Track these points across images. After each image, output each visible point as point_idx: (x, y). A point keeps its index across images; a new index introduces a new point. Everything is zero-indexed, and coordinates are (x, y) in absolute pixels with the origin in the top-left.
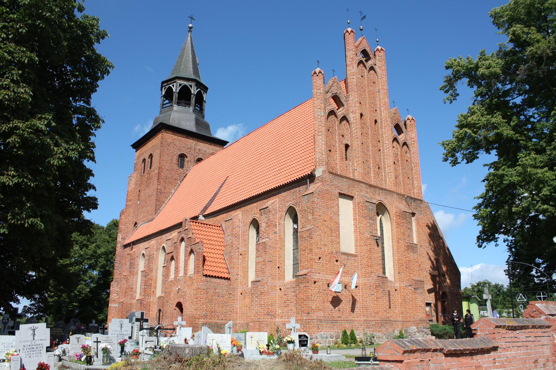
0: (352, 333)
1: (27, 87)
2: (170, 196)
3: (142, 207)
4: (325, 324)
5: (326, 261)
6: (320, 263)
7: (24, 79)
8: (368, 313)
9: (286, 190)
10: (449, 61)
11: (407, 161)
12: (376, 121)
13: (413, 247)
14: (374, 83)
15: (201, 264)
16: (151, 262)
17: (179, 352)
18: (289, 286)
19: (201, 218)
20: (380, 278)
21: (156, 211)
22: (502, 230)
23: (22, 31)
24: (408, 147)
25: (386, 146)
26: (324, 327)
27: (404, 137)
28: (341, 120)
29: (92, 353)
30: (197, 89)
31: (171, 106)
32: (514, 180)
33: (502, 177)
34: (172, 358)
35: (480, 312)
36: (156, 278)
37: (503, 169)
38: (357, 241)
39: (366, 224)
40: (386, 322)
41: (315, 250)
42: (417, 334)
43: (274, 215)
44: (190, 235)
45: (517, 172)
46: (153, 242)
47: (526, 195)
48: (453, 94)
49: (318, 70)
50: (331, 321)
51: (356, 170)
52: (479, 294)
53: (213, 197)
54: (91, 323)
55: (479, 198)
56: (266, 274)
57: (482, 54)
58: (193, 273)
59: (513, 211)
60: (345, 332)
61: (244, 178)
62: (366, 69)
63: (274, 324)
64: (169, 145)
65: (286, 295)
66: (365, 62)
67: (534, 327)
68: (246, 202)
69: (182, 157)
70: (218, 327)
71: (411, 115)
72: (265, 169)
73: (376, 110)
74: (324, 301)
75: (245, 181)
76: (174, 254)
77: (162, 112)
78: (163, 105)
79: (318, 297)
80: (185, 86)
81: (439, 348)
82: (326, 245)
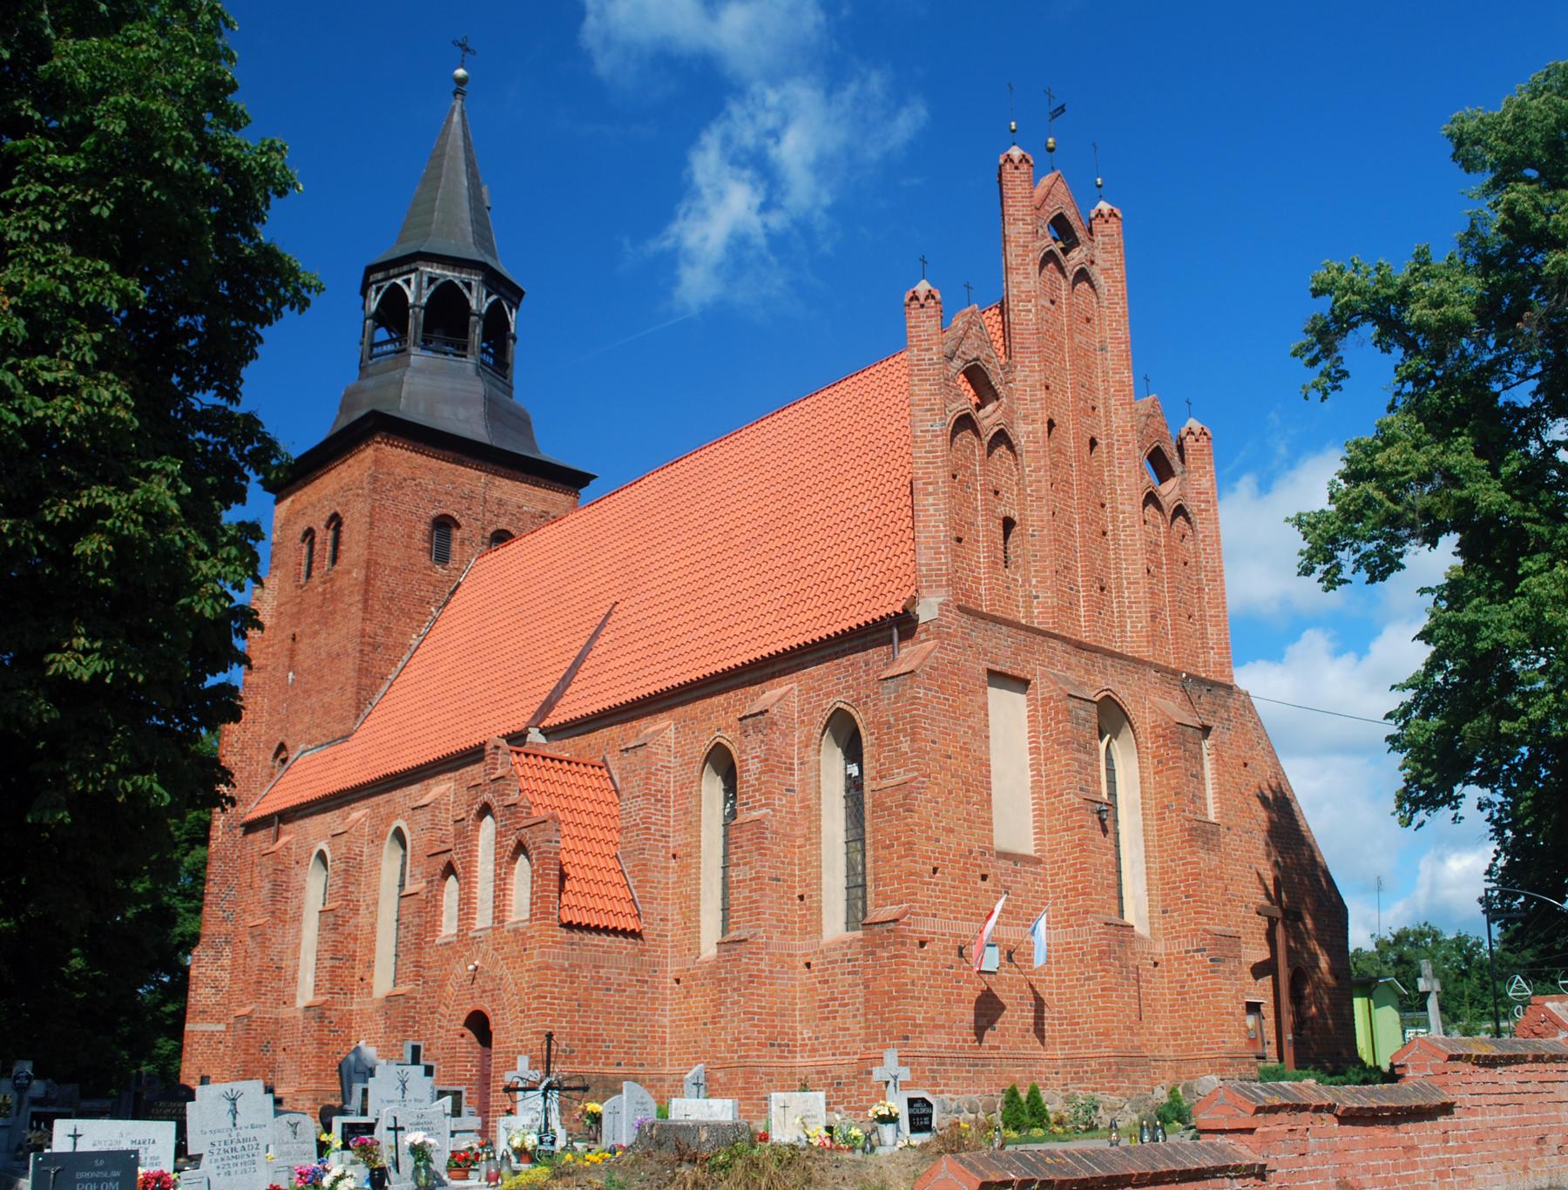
0: (1034, 1095)
1: (118, 383)
2: (405, 658)
3: (306, 691)
4: (953, 1071)
5: (953, 880)
6: (937, 885)
7: (107, 359)
8: (1077, 1036)
9: (824, 657)
10: (1322, 273)
11: (1185, 564)
12: (1093, 443)
13: (1206, 832)
14: (1088, 320)
15: (553, 887)
16: (352, 880)
18: (837, 955)
19: (535, 736)
20: (1112, 930)
21: (358, 708)
22: (1474, 773)
23: (99, 214)
24: (1188, 520)
25: (1124, 521)
26: (950, 1079)
27: (1177, 491)
31: (404, 350)
32: (1508, 640)
33: (1472, 629)
34: (668, 1154)
35: (1404, 1032)
36: (373, 932)
37: (1476, 607)
38: (1041, 816)
39: (1068, 765)
40: (1130, 1062)
41: (923, 847)
43: (785, 735)
44: (514, 797)
45: (1516, 616)
46: (358, 813)
47: (1541, 685)
48: (1333, 371)
50: (971, 1061)
51: (1037, 597)
52: (1400, 970)
53: (570, 669)
54: (513, 1067)
55: (1403, 687)
56: (765, 920)
57: (1422, 258)
58: (527, 916)
59: (1503, 730)
60: (1013, 1093)
62: (1065, 277)
63: (791, 1074)
64: (399, 487)
65: (826, 982)
66: (1060, 255)
67: (1538, 1059)
68: (691, 690)
69: (444, 525)
70: (605, 1087)
72: (746, 584)
73: (1094, 408)
74: (949, 1001)
75: (681, 620)
77: (370, 370)
78: (373, 345)
79: (931, 987)
80: (450, 284)
81: (1326, 1103)
82: (952, 831)
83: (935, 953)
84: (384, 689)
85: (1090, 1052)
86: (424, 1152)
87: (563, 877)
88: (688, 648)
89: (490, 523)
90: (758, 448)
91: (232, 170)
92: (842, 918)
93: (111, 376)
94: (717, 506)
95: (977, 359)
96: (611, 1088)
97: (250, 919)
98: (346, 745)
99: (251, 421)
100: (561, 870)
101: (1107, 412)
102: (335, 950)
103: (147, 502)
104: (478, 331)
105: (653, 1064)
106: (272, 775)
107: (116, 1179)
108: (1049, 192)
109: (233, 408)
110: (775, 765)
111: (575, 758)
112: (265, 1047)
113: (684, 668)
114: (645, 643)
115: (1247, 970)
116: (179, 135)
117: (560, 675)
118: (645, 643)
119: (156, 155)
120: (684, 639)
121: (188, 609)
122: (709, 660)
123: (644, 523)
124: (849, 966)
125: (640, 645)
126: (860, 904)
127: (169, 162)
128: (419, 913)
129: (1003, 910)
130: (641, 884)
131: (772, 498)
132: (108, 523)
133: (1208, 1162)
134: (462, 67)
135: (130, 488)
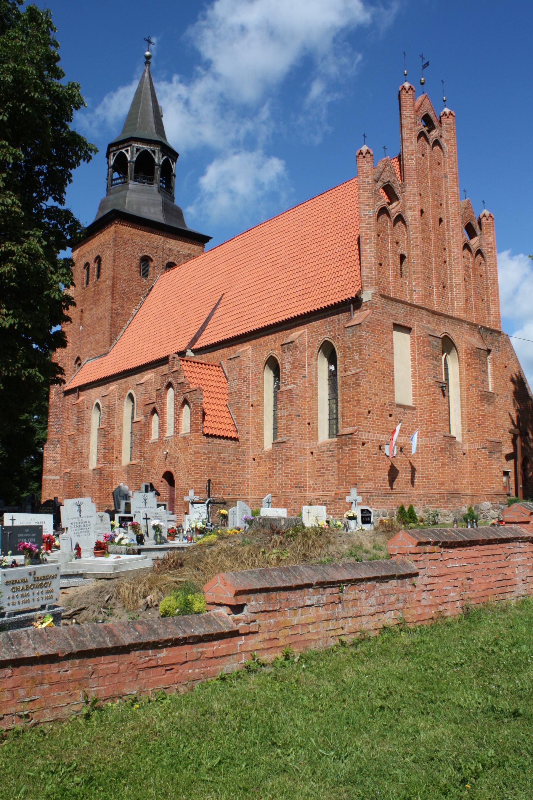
0: (411, 509)
2: (130, 319)
3: (88, 334)
12: (441, 220)
13: (488, 396)
14: (439, 164)
15: (200, 418)
17: (275, 524)
18: (325, 449)
19: (189, 353)
20: (446, 439)
24: (483, 256)
27: (478, 243)
28: (395, 220)
29: (143, 531)
30: (163, 157)
31: (126, 182)
34: (267, 530)
42: (492, 511)
46: (113, 387)
49: (364, 148)
51: (415, 291)
53: (204, 324)
54: (187, 495)
58: (189, 431)
60: (402, 508)
61: (251, 298)
62: (429, 143)
64: (126, 243)
65: (320, 460)
69: (145, 260)
71: (488, 210)
72: (283, 285)
73: (441, 205)
74: (374, 469)
75: (253, 301)
76: (157, 405)
77: (112, 191)
80: (146, 151)
82: (377, 395)
83: (369, 448)
84: (121, 333)
85: (436, 491)
86: (159, 529)
87: (204, 414)
88: (257, 314)
89: (166, 259)
90: (287, 224)
91: (56, 97)
92: (327, 432)
93: (11, 193)
94: (269, 250)
95: (389, 182)
96: (234, 503)
97: (68, 432)
98: (106, 358)
99: (68, 214)
100: (203, 411)
101: (447, 206)
102: (105, 445)
103: (30, 249)
104: (159, 173)
105: (243, 495)
106: (74, 371)
107: (34, 537)
108: (422, 104)
109: (60, 207)
110: (297, 365)
111: (207, 363)
112: (77, 486)
113: (256, 323)
114: (237, 312)
115: (503, 457)
116: (36, 82)
117: (200, 326)
118: (237, 312)
119: (27, 91)
120: (255, 310)
121: (48, 296)
122: (267, 319)
123: (235, 258)
124: (330, 454)
125: (235, 312)
126: (335, 427)
127: (32, 94)
128: (141, 429)
129: (400, 430)
130: (238, 417)
131: (294, 246)
132: (14, 258)
133: (510, 536)
134: (148, 51)
135: (21, 243)
